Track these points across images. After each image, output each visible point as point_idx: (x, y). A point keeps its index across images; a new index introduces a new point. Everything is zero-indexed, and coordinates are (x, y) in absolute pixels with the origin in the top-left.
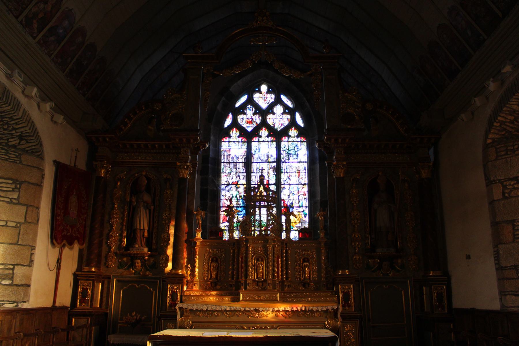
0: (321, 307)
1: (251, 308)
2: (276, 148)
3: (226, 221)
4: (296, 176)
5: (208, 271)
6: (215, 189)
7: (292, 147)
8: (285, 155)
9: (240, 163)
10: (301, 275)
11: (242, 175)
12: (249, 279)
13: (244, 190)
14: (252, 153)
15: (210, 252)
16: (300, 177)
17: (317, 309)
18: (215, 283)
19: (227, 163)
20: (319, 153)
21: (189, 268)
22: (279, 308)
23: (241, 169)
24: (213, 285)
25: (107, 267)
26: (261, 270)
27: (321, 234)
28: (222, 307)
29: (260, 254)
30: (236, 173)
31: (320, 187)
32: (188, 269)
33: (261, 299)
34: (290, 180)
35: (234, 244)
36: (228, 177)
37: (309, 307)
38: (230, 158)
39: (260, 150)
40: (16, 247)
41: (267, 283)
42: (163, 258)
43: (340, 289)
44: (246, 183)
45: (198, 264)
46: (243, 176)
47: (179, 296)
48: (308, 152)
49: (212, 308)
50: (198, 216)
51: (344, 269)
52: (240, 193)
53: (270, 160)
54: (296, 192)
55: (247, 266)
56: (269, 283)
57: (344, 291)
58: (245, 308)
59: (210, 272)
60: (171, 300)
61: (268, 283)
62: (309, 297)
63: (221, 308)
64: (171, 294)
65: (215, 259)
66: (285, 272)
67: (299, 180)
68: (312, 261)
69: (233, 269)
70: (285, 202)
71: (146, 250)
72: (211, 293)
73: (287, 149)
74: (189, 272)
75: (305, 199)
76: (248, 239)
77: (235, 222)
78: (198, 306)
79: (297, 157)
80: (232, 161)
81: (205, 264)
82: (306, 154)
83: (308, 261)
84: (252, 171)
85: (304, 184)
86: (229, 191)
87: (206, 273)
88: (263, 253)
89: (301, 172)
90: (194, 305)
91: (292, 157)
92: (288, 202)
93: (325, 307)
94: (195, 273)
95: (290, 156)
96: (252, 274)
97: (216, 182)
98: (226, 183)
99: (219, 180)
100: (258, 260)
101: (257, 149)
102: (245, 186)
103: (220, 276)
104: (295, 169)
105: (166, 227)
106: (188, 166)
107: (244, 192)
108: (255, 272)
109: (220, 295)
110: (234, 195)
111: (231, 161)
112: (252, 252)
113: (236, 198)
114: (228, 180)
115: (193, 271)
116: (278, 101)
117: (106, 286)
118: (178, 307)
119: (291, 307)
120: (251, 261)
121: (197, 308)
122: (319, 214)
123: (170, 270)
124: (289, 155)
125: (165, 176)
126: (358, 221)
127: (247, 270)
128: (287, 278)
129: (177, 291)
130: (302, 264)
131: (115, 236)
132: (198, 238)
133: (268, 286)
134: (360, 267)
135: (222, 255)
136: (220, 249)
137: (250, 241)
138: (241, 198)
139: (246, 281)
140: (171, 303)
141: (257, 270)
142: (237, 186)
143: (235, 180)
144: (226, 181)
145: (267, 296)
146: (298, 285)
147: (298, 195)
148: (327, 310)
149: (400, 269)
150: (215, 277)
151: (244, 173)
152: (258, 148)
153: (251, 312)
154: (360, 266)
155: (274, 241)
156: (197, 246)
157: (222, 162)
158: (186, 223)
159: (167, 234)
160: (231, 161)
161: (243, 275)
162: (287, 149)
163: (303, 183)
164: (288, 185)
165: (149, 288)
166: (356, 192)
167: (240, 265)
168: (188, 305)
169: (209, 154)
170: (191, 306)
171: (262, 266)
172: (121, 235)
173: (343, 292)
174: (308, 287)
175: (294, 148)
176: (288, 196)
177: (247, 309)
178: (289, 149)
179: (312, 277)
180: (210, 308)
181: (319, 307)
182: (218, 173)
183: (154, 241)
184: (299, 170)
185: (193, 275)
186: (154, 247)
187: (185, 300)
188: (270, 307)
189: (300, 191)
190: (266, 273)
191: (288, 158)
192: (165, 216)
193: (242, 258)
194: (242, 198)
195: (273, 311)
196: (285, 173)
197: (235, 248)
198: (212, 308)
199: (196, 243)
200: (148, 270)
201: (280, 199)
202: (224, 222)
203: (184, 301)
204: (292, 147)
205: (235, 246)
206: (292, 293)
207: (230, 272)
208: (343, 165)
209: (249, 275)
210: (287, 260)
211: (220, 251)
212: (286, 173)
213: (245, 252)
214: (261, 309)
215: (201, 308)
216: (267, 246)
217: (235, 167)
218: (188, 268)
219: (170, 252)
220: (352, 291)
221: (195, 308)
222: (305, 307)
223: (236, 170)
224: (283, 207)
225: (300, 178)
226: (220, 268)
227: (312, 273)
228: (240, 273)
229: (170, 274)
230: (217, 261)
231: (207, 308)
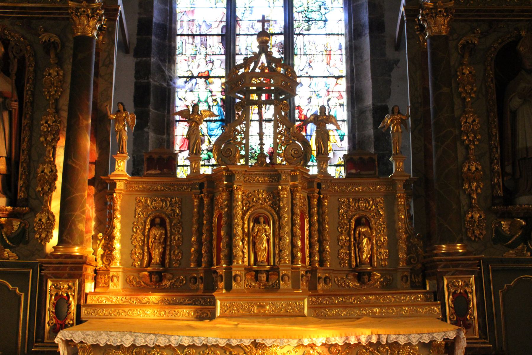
0: (416, 335)
1: (245, 340)
2: (285, 7)
3: (186, 149)
4: (323, 61)
5: (142, 248)
6: (165, 85)
7: (314, 5)
8: (301, 22)
9: (213, 35)
10: (353, 255)
11: (218, 59)
12: (236, 267)
13: (223, 88)
14: (237, 17)
15: (149, 206)
16: (332, 63)
17: (406, 339)
18: (159, 273)
19: (188, 35)
20: (370, 14)
21: (101, 242)
22: (314, 339)
23: (215, 47)
24: (154, 278)
26: (264, 245)
27: (396, 165)
28: (172, 339)
29: (262, 208)
30: (206, 55)
31: (372, 81)
32: (97, 243)
33: (265, 311)
34: (311, 69)
35: (201, 186)
36: (189, 63)
37: (388, 335)
38: (195, 27)
39: (251, 10)
41: (279, 275)
42: (40, 220)
43: (446, 288)
44: (226, 74)
45: (121, 231)
46: (220, 62)
47: (73, 307)
48: (347, 15)
49: (146, 341)
50: (119, 124)
51: (452, 241)
52: (213, 94)
54: (323, 93)
55: (231, 235)
56: (285, 275)
57: (455, 292)
58: (229, 340)
59: (148, 248)
60: (54, 317)
61: (281, 275)
62: (375, 307)
63: (170, 341)
64: (54, 303)
65: (158, 220)
66: (317, 249)
67: (329, 69)
68: (375, 224)
69: (200, 243)
70: (302, 111)
72: (149, 297)
73: (306, 9)
74: (100, 251)
75: (341, 105)
76: (234, 172)
77: (203, 151)
78: (111, 336)
79: (325, 24)
80: (198, 33)
81: (136, 233)
82: (343, 19)
83: (368, 224)
84: (237, 52)
85: (338, 78)
86: (191, 91)
87: (139, 253)
88: (269, 205)
89: (332, 53)
90: (100, 335)
91: (316, 24)
92: (308, 111)
93: (427, 335)
94: (114, 253)
95: (310, 23)
96: (243, 252)
97: (167, 72)
98: (186, 75)
99: (172, 68)
100: (257, 221)
101: (248, 8)
102: (224, 80)
103: (170, 259)
104: (321, 48)
105: (48, 149)
106: (94, 11)
107: (222, 92)
108: (251, 249)
109: (169, 304)
110: (203, 99)
111: (196, 31)
112: (244, 202)
113: (206, 104)
114: (190, 68)
115: (108, 248)
118: (61, 339)
119: (343, 335)
120: (241, 224)
121: (109, 340)
122: (391, 121)
123: (53, 247)
124: (309, 21)
125: (45, 37)
126: (475, 137)
127: (230, 246)
128: (322, 262)
129: (68, 296)
130: (355, 230)
132: (120, 173)
133: (281, 283)
134: (481, 237)
135: (174, 211)
136: (169, 199)
137: (237, 177)
138: (215, 104)
139: (229, 270)
140: (55, 325)
141: (254, 245)
142: (207, 80)
143: (203, 69)
144: (187, 71)
145: (281, 304)
146: (347, 276)
147: (327, 98)
149: (11, 245)
150: (159, 260)
151: (221, 54)
152: (250, 7)
153: (242, 348)
154: (481, 233)
155: (294, 178)
156: (116, 191)
157: (178, 35)
158: (91, 138)
159: (49, 165)
160: (196, 31)
161: (222, 256)
162: (306, 9)
163: (337, 75)
164: (308, 79)
165: (11, 287)
166: (470, 72)
167: (215, 234)
168: (87, 335)
169: (152, 17)
170: (93, 336)
171: (266, 235)
173: (454, 294)
174: (369, 281)
175: (319, 8)
176: (308, 99)
177: (234, 342)
178: (309, 11)
179: (377, 258)
181: (413, 335)
183: (20, 183)
184: (329, 49)
185: (108, 256)
186: (21, 195)
187: (87, 317)
188: (291, 338)
189: (330, 90)
190: (277, 252)
191: (306, 27)
192: (46, 127)
193: (220, 217)
194: (218, 103)
195: (300, 345)
196: (301, 54)
197: (202, 195)
198: (146, 341)
199: (115, 184)
200: (6, 246)
201: (292, 106)
202: (183, 149)
203: (84, 320)
204: (314, 5)
205: (204, 190)
206: (336, 296)
207: (193, 249)
208: (447, 10)
209: (236, 256)
210: (321, 222)
211: (170, 201)
212: (304, 55)
213: (227, 204)
214: (268, 343)
215: (119, 340)
216: (278, 188)
218: (99, 242)
219: (55, 206)
220: (472, 292)
221: (105, 341)
222: (379, 335)
223: (206, 49)
224: (297, 121)
225: (331, 64)
226: (170, 242)
227: (377, 250)
228: (215, 251)
229: (54, 255)
230: (162, 224)
231: (134, 340)
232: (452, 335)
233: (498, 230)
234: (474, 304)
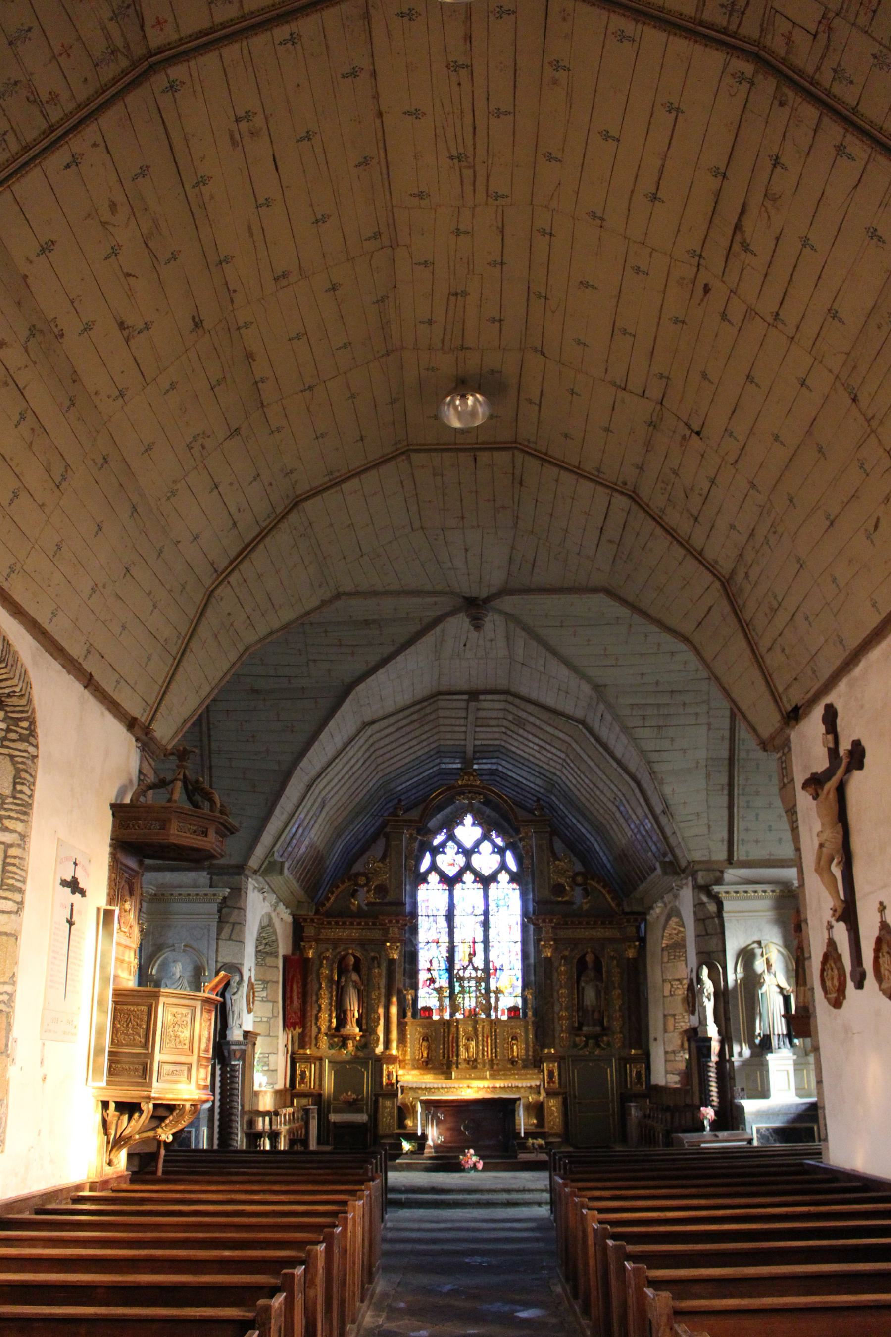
25: (318, 1048)
40: (269, 1039)
51: (550, 1048)
53: (475, 913)
55: (458, 1046)
71: (357, 1030)
83: (516, 1039)
100: (468, 1040)
116: (486, 837)
117: (318, 1067)
125: (372, 954)
127: (458, 1050)
128: (496, 1056)
131: (324, 1015)
139: (457, 1060)
141: (467, 1049)
148: (531, 1087)
172: (330, 1015)
180: (428, 1086)
182: (414, 930)
186: (364, 1027)
210: (496, 1039)
217: (435, 921)
230: (427, 1040)
232: (538, 1084)
233: (574, 1042)
234: (556, 1074)
